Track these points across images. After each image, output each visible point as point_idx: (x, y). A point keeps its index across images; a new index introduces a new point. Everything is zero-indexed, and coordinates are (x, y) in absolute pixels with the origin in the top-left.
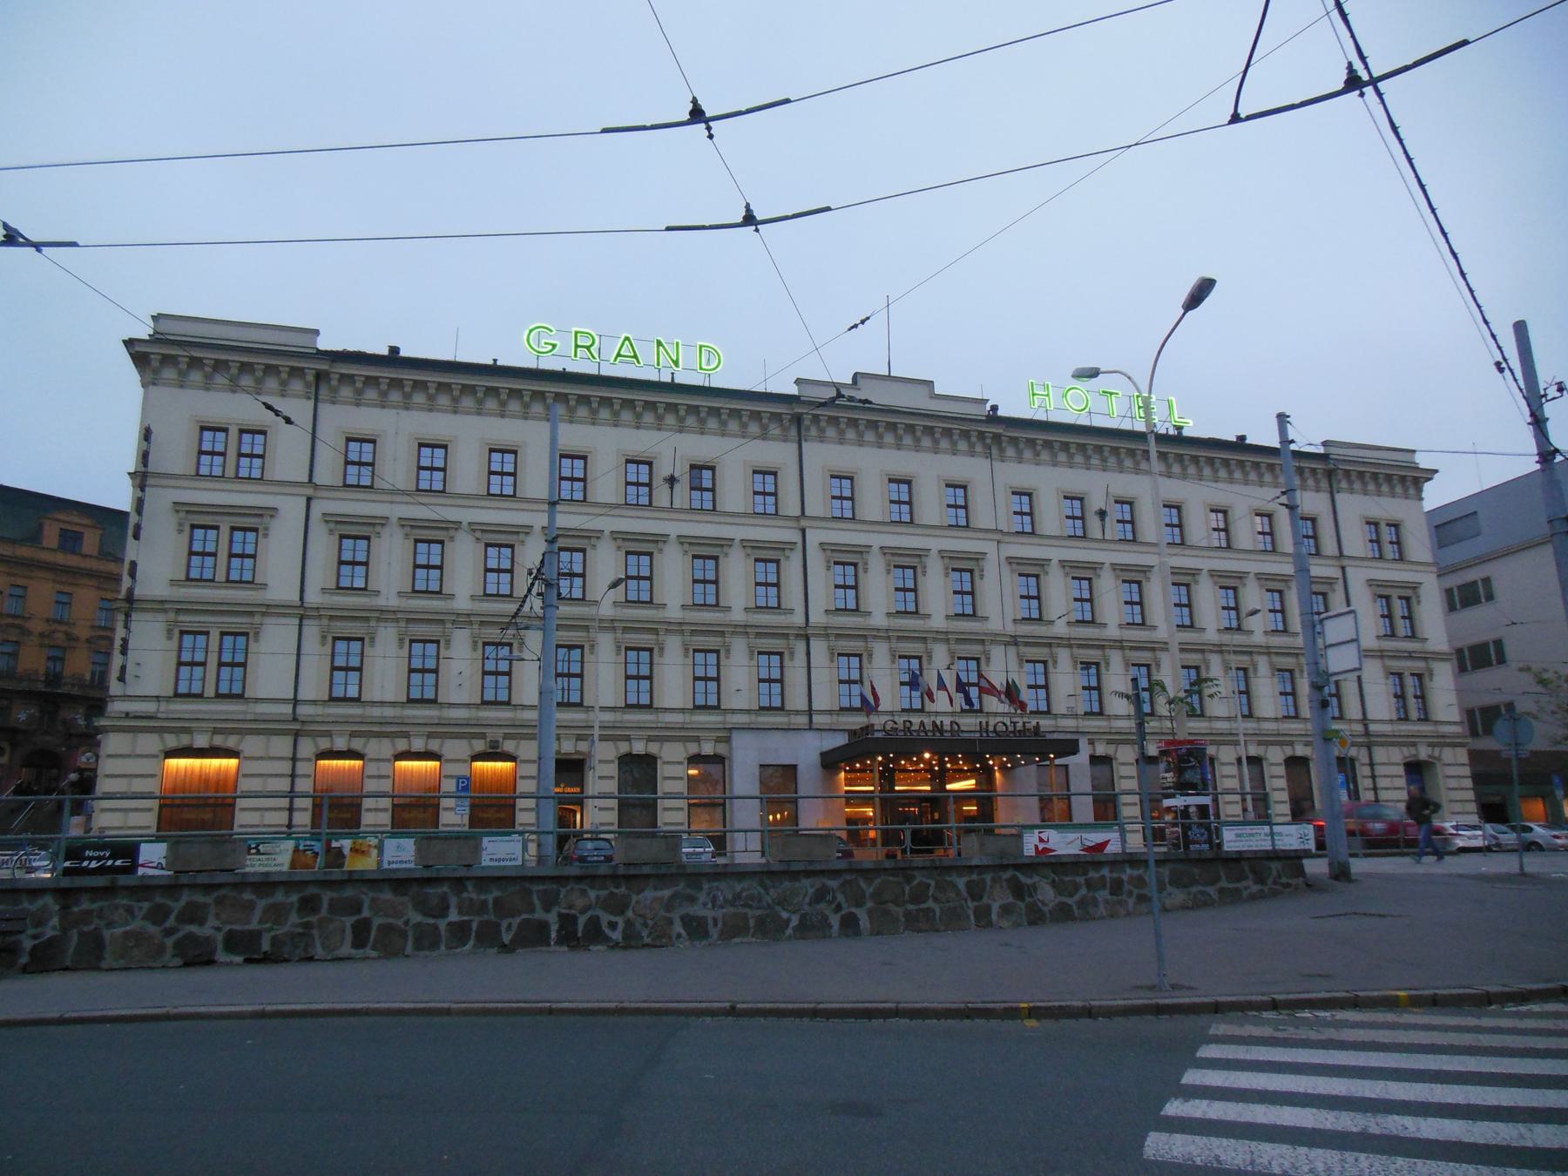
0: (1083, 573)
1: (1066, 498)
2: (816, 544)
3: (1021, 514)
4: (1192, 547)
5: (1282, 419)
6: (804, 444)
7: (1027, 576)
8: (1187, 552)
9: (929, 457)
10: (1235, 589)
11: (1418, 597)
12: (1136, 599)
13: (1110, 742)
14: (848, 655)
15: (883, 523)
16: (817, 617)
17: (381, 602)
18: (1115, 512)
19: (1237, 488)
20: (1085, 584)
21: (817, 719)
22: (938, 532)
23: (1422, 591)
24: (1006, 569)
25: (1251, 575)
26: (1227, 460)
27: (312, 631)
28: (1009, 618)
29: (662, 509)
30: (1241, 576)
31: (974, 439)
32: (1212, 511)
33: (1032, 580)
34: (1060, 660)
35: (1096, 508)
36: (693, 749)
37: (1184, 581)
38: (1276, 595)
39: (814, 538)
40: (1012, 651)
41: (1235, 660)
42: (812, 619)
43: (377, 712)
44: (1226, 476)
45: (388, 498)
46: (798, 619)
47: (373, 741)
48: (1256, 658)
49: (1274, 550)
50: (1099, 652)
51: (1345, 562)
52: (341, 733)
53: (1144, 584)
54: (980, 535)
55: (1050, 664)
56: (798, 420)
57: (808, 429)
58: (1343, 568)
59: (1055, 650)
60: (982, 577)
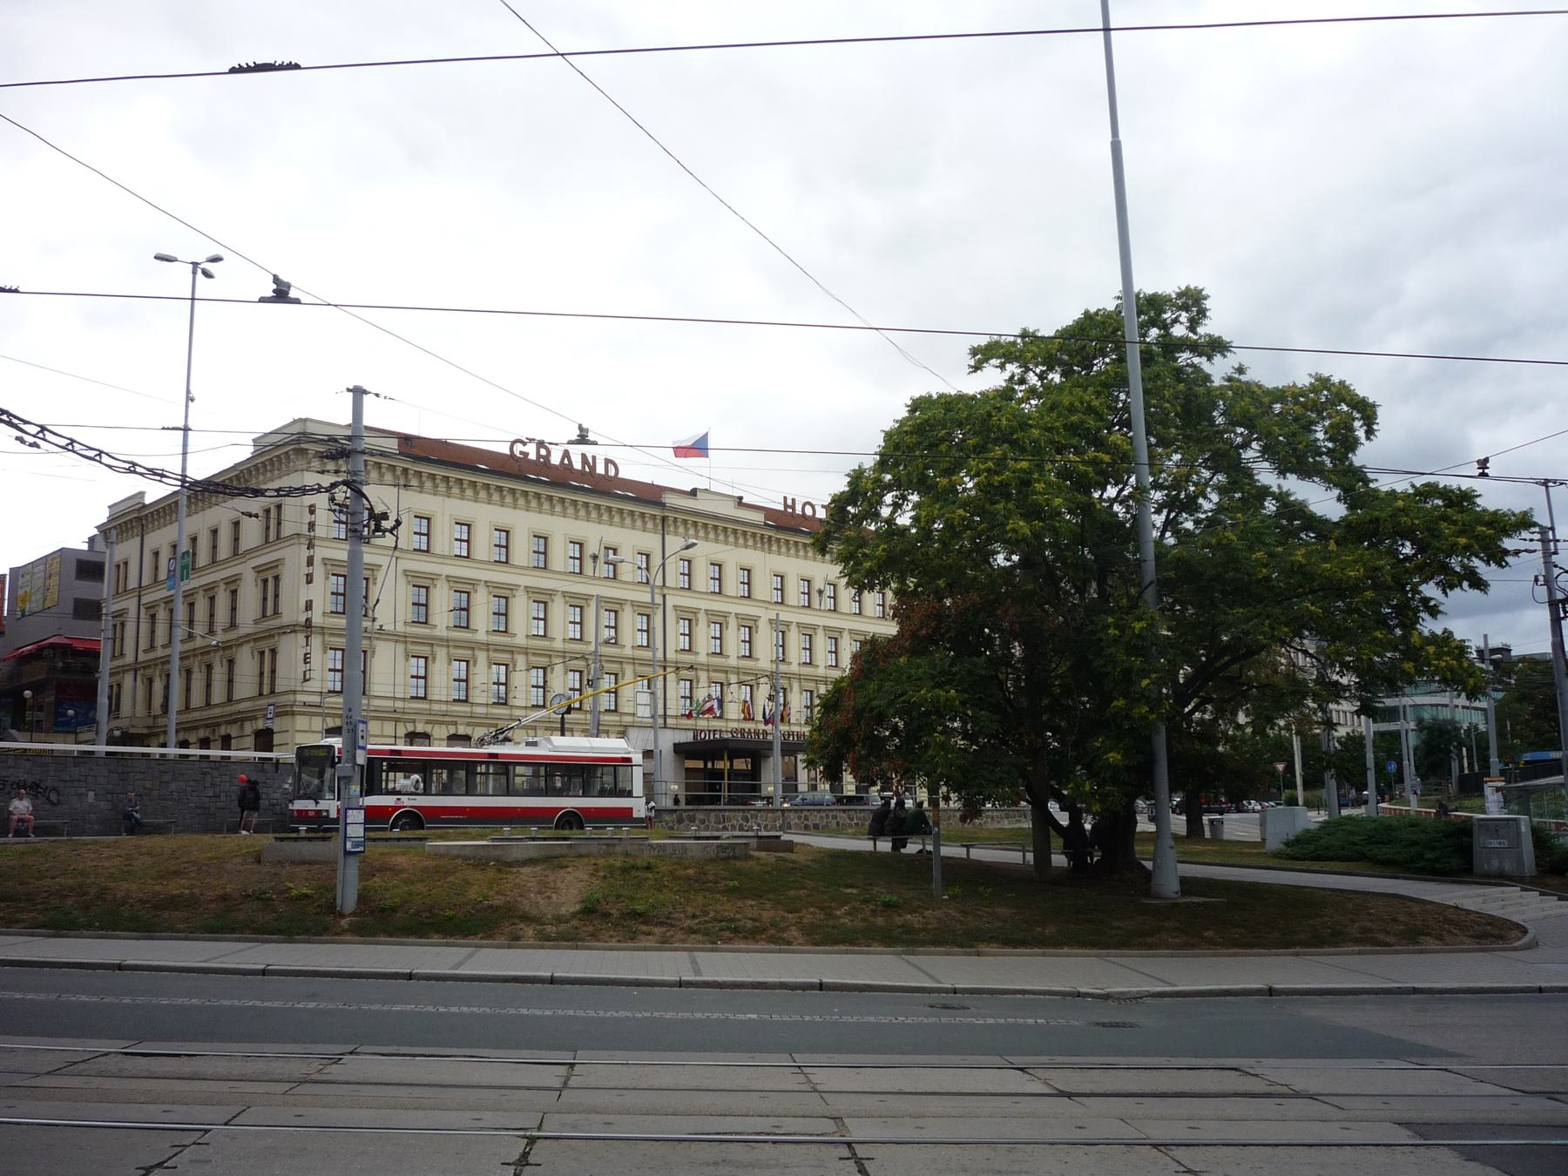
0: (809, 632)
1: (535, 536)
2: (320, 559)
3: (538, 552)
4: (755, 600)
5: (1486, 636)
6: (666, 536)
7: (419, 587)
8: (863, 620)
9: (793, 560)
10: (545, 603)
11: (757, 628)
12: (542, 616)
13: (468, 724)
14: (460, 661)
15: (676, 589)
16: (671, 655)
17: (437, 633)
18: (416, 525)
19: (438, 499)
20: (503, 601)
21: (669, 721)
22: (734, 601)
23: (380, 576)
24: (402, 580)
25: (522, 588)
26: (686, 520)
27: (316, 641)
28: (401, 618)
29: (815, 609)
30: (513, 588)
31: (758, 539)
32: (571, 542)
33: (464, 596)
34: (438, 656)
35: (591, 553)
36: (452, 730)
37: (465, 589)
38: (503, 601)
39: (670, 601)
40: (400, 648)
41: (684, 673)
42: (668, 656)
43: (436, 707)
44: (485, 496)
45: (441, 561)
46: (660, 655)
47: (437, 727)
48: (436, 649)
49: (749, 597)
50: (428, 648)
51: (666, 591)
52: (420, 721)
53: (550, 604)
54: (518, 571)
55: (471, 663)
56: (664, 519)
57: (669, 526)
58: (664, 596)
59: (476, 652)
60: (727, 628)
